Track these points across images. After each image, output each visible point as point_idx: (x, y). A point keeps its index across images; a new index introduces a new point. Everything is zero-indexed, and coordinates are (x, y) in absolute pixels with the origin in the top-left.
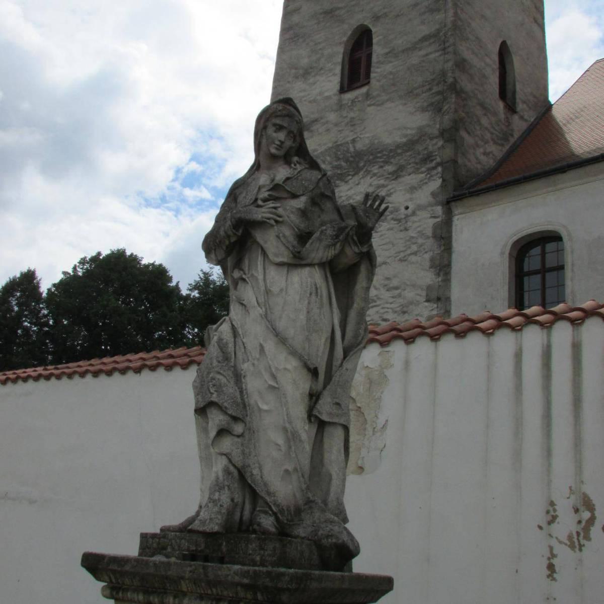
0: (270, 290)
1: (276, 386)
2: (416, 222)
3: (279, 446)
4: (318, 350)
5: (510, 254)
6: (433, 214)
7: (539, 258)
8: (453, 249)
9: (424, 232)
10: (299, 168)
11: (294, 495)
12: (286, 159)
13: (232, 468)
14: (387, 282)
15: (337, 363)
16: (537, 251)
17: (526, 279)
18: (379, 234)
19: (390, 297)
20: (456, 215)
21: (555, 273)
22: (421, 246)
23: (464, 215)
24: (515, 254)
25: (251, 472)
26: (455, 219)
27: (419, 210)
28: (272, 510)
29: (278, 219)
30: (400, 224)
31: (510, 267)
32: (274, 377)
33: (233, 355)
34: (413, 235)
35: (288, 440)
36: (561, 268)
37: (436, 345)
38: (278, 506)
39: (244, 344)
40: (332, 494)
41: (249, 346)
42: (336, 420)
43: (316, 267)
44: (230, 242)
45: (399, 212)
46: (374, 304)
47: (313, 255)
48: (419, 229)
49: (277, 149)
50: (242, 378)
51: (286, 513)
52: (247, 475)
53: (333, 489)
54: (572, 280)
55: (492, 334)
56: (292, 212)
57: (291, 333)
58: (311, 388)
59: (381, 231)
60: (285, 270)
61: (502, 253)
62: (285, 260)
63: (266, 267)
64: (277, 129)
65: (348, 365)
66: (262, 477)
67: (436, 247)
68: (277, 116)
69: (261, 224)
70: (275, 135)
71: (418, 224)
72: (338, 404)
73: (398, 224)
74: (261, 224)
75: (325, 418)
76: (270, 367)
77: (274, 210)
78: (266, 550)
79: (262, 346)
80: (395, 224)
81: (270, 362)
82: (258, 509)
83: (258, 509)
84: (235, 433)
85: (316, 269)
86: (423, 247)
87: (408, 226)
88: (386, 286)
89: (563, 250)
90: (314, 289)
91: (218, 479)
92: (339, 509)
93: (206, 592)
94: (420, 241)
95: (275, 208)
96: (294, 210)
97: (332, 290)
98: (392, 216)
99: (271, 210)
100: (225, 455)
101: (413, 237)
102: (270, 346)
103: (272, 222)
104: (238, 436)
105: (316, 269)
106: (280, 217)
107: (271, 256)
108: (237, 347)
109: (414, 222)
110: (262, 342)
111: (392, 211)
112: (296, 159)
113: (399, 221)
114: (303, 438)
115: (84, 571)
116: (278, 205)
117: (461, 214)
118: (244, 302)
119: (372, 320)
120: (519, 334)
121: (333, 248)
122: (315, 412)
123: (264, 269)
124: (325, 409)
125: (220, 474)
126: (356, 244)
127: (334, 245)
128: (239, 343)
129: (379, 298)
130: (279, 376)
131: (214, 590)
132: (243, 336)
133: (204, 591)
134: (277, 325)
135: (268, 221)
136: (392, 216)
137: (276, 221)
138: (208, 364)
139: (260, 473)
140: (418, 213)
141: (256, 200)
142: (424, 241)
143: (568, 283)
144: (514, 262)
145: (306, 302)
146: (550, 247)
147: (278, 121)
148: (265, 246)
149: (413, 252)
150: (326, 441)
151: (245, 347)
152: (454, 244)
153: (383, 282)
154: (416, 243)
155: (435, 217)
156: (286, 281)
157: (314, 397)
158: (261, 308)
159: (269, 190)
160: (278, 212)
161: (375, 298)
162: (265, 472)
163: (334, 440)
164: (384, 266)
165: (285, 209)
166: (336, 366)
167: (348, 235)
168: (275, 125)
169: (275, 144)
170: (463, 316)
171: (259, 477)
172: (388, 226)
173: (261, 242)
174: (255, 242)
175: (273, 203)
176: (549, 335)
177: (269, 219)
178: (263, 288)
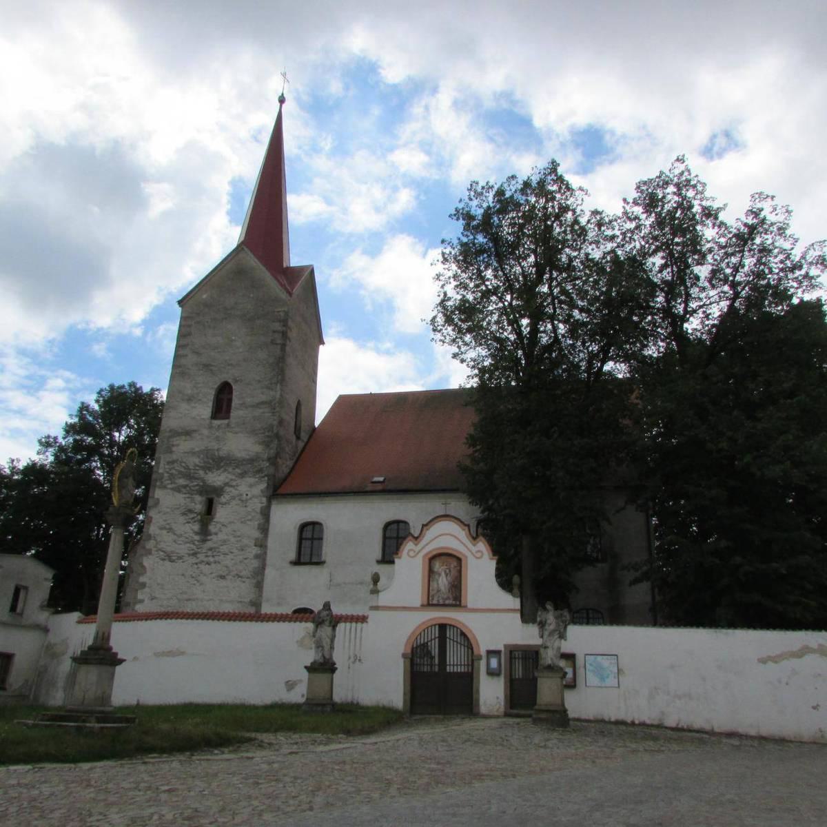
14: (233, 533)
89: (321, 539)
94: (253, 514)
155: (262, 503)
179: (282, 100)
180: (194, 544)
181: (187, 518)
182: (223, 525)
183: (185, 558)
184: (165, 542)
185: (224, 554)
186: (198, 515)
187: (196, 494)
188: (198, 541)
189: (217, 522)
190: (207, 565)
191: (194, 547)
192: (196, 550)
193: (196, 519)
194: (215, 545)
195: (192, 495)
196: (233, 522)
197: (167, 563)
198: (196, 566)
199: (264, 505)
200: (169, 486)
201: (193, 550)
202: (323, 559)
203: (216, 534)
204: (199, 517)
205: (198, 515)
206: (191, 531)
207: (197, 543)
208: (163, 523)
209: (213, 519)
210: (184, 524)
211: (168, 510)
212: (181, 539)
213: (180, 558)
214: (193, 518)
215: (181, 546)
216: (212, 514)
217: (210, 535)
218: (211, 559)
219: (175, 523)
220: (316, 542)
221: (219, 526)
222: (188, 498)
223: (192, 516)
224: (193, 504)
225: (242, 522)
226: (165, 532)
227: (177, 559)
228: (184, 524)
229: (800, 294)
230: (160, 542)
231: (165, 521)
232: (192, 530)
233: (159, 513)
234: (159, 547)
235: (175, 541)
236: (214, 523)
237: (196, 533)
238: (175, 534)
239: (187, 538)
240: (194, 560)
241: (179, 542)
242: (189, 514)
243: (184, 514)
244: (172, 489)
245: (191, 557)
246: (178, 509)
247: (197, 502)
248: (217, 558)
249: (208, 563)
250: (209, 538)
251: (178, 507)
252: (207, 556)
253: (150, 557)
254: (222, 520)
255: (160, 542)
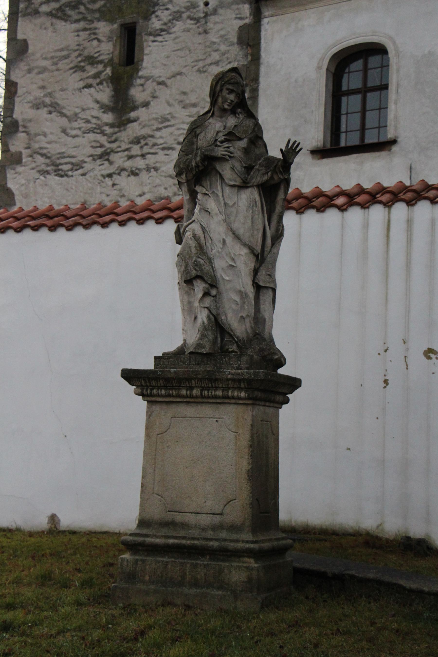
0: (227, 203)
1: (235, 265)
2: (217, 23)
3: (237, 301)
4: (257, 242)
5: (328, 69)
6: (240, 14)
7: (360, 75)
8: (262, 61)
9: (227, 37)
10: (241, 116)
11: (247, 332)
12: (233, 112)
13: (211, 316)
14: (182, 97)
15: (267, 249)
16: (358, 65)
17: (344, 99)
18: (173, 36)
19: (187, 116)
20: (265, 17)
21: (378, 93)
22: (224, 54)
23: (274, 18)
24: (333, 69)
25: (221, 318)
26: (265, 21)
27: (222, 8)
28: (235, 340)
29: (231, 155)
30: (198, 24)
31: (327, 85)
32: (233, 260)
33: (205, 245)
34: (215, 40)
35: (242, 298)
36: (385, 87)
37: (300, 219)
38: (237, 338)
39: (211, 238)
40: (266, 330)
41: (214, 239)
42: (268, 285)
43: (255, 187)
44: (199, 170)
45: (198, 9)
46: (169, 123)
47: (254, 180)
48: (222, 33)
49: (228, 105)
50: (212, 261)
51: (242, 341)
52: (219, 320)
53: (267, 327)
54: (396, 103)
55: (346, 210)
56: (239, 150)
57: (241, 232)
58: (255, 266)
59: (174, 32)
60: (236, 189)
61: (319, 68)
62: (237, 184)
63: (223, 188)
64: (229, 92)
65: (274, 250)
66: (227, 321)
67: (241, 56)
68: (230, 84)
69: (222, 159)
70: (228, 96)
71: (219, 26)
72: (269, 275)
73: (196, 24)
74: (222, 159)
75: (261, 284)
76: (230, 254)
77: (228, 149)
78: (242, 361)
79: (224, 241)
80: (191, 24)
81: (230, 250)
82: (226, 340)
83: (226, 340)
84: (212, 295)
85: (254, 189)
86: (226, 56)
87: (208, 28)
88: (181, 101)
89: (388, 66)
90: (254, 202)
91: (204, 322)
92: (270, 339)
93: (208, 386)
94: (223, 48)
95: (228, 147)
96: (240, 148)
97: (264, 202)
98: (188, 13)
99: (226, 149)
100: (207, 308)
101: (214, 43)
102: (229, 240)
103: (227, 157)
104: (213, 296)
105: (254, 189)
106: (231, 153)
107: (227, 181)
108: (206, 240)
109: (215, 23)
110: (224, 237)
111: (189, 6)
112: (239, 110)
113: (197, 20)
114: (250, 297)
115: (123, 379)
116: (231, 145)
117: (272, 16)
118: (208, 210)
119: (165, 143)
120: (367, 210)
121: (266, 175)
122: (256, 281)
123: (222, 188)
124: (262, 280)
125: (206, 321)
126: (281, 173)
127: (267, 173)
128: (207, 237)
129: (173, 117)
130: (236, 259)
131: (214, 384)
132: (210, 233)
133: (207, 385)
134: (233, 226)
135: (224, 157)
136: (188, 13)
137: (230, 157)
138: (188, 251)
139: (225, 318)
140: (221, 11)
141: (216, 140)
142: (228, 48)
143: (392, 106)
144: (331, 79)
145: (251, 212)
146: (374, 61)
147: (230, 87)
148: (222, 173)
149: (214, 61)
150: (261, 298)
151: (211, 240)
152: (263, 54)
153: (177, 97)
154: (217, 50)
155: (241, 19)
156: (237, 198)
157: (256, 271)
158: (222, 215)
159: (224, 135)
160: (231, 151)
161: (169, 117)
162: (229, 319)
163: (266, 297)
164: (178, 77)
165: (234, 148)
166: (267, 251)
167: (275, 167)
168: (228, 89)
169: (228, 102)
170: (317, 189)
171: (225, 321)
172: (184, 27)
173: (220, 171)
174: (215, 169)
175: (227, 144)
176: (389, 213)
177: (225, 155)
178: (222, 202)
179: (67, 99)
180: (103, 133)
181: (85, 75)
182: (160, 83)
183: (87, 167)
184: (45, 135)
185: (163, 149)
186: (105, 67)
187: (99, 20)
188: (112, 126)
189: (147, 78)
190: (132, 177)
191: (103, 140)
192: (108, 145)
193: (103, 76)
194: (146, 131)
195: (92, 21)
196: (180, 74)
197: (53, 179)
198: (109, 182)
199: (247, 21)
200: (45, 8)
201: (101, 146)
202: (390, 135)
203: (146, 105)
204: (109, 71)
205: (105, 67)
206: (97, 106)
207: (108, 130)
208: (40, 94)
209: (138, 70)
210: (80, 90)
211: (45, 63)
212: (75, 125)
213: (78, 166)
214: (96, 76)
215: (77, 139)
216: (136, 60)
217: (135, 108)
218: (140, 163)
219: (62, 90)
220: (384, 69)
221: (150, 86)
222: (85, 29)
223: (92, 71)
224: (95, 43)
225: (199, 71)
226: (43, 112)
227: (71, 170)
228: (80, 90)
229: (242, 363)
230: (37, 135)
231: (43, 87)
232: (97, 102)
233: (29, 71)
234: (36, 146)
235: (64, 131)
236: (139, 81)
237: (105, 108)
238: (63, 115)
239: (88, 121)
240: (107, 169)
241: (74, 132)
242: (88, 68)
243: (78, 68)
244: (50, 14)
245: (99, 162)
246: (66, 57)
247: (102, 38)
248: (151, 160)
249: (134, 173)
250: (133, 115)
251: (65, 53)
252: (130, 157)
253: (20, 169)
254: (156, 73)
255: (37, 135)
